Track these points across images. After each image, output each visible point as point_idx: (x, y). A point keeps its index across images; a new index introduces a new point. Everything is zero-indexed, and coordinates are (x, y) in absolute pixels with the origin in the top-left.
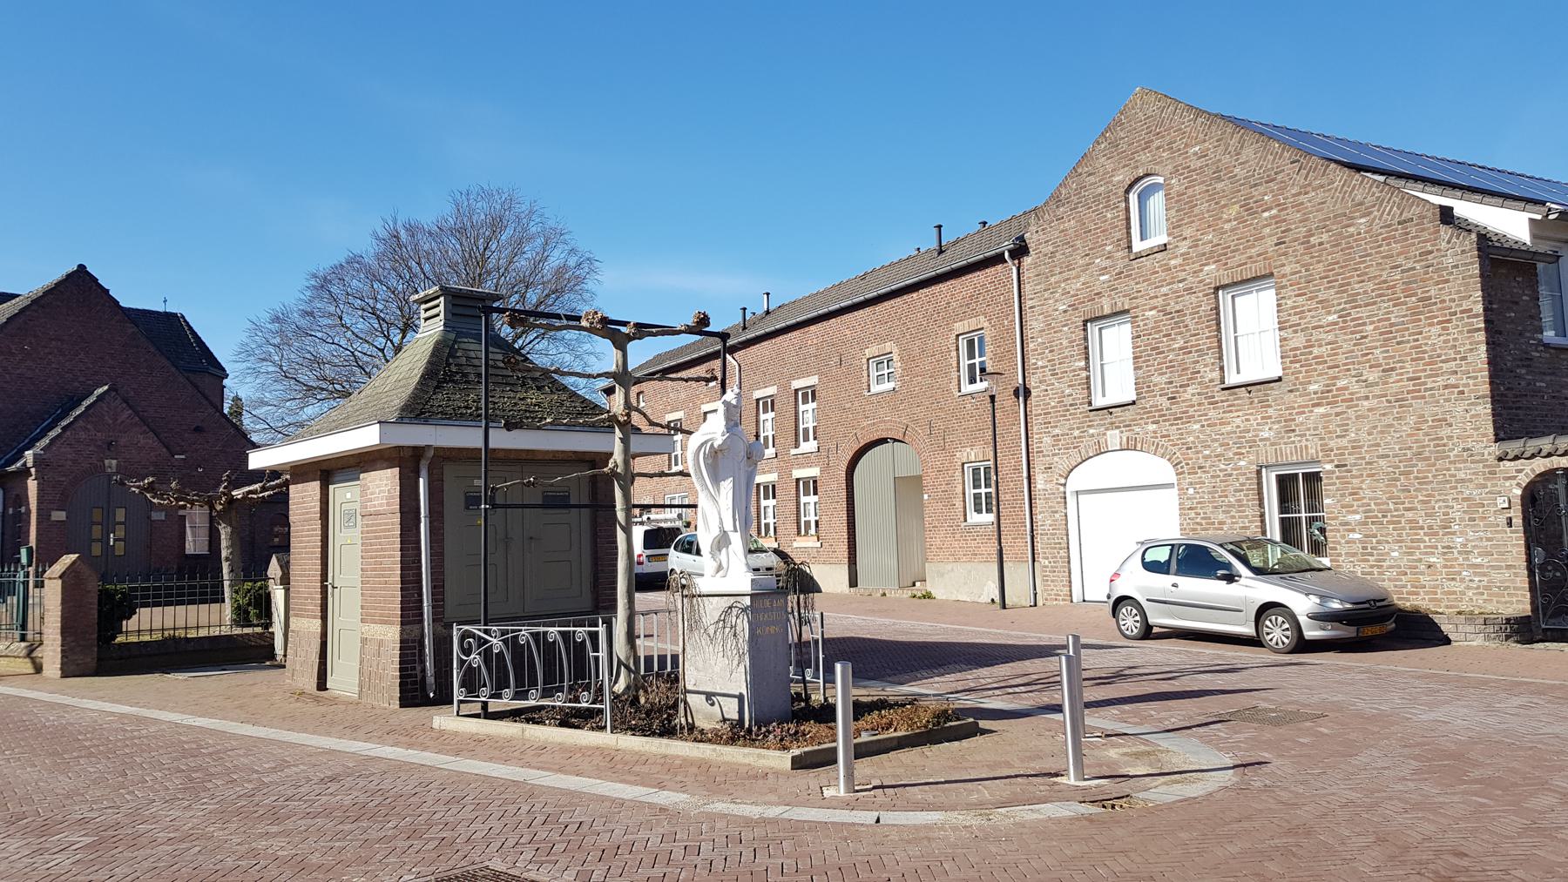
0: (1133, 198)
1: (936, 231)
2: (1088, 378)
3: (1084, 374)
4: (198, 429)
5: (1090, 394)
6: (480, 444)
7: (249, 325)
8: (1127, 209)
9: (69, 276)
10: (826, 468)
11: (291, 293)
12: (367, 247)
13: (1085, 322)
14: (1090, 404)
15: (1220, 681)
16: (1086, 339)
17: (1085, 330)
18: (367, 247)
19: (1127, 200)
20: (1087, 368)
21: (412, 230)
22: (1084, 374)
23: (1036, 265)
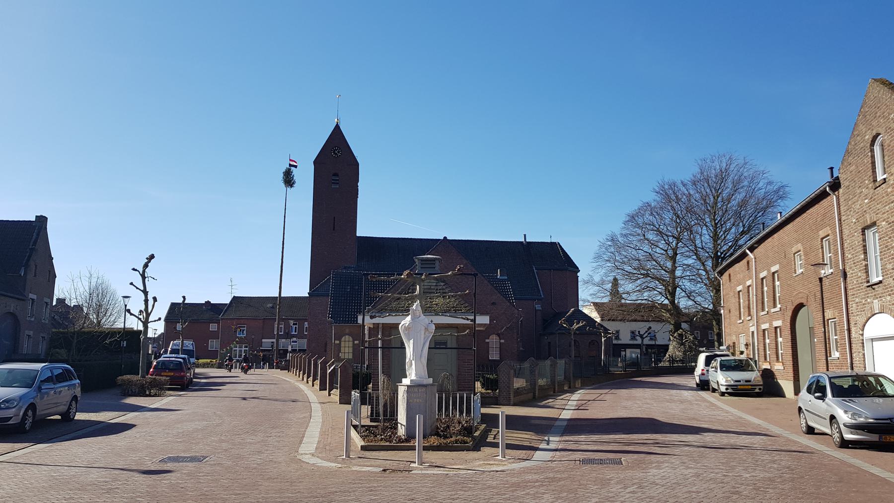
0: (877, 149)
1: (829, 171)
2: (866, 265)
3: (864, 263)
4: (493, 304)
5: (868, 276)
6: (477, 318)
7: (599, 243)
8: (873, 157)
9: (208, 305)
10: (783, 321)
11: (616, 226)
12: (651, 197)
13: (863, 230)
14: (868, 282)
15: (228, 380)
16: (864, 240)
17: (864, 234)
18: (651, 197)
19: (872, 151)
20: (866, 259)
21: (672, 186)
22: (864, 263)
23: (844, 194)
